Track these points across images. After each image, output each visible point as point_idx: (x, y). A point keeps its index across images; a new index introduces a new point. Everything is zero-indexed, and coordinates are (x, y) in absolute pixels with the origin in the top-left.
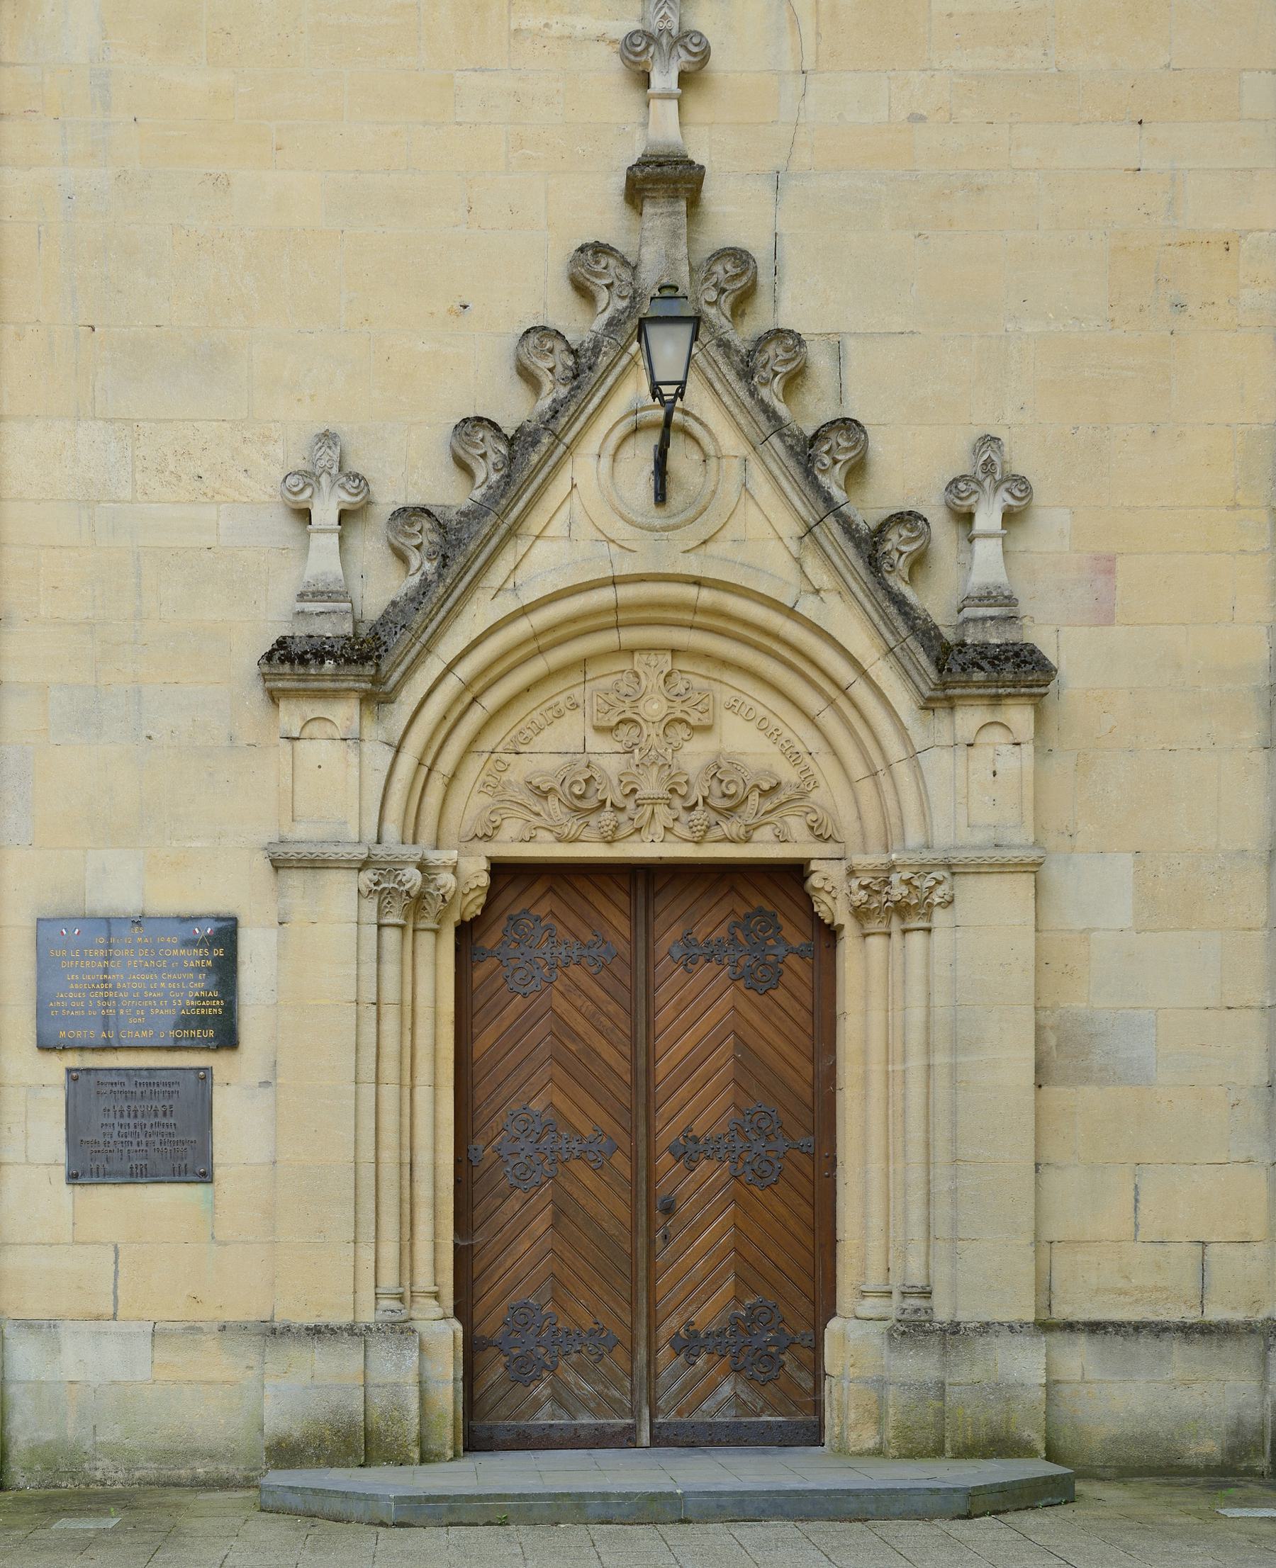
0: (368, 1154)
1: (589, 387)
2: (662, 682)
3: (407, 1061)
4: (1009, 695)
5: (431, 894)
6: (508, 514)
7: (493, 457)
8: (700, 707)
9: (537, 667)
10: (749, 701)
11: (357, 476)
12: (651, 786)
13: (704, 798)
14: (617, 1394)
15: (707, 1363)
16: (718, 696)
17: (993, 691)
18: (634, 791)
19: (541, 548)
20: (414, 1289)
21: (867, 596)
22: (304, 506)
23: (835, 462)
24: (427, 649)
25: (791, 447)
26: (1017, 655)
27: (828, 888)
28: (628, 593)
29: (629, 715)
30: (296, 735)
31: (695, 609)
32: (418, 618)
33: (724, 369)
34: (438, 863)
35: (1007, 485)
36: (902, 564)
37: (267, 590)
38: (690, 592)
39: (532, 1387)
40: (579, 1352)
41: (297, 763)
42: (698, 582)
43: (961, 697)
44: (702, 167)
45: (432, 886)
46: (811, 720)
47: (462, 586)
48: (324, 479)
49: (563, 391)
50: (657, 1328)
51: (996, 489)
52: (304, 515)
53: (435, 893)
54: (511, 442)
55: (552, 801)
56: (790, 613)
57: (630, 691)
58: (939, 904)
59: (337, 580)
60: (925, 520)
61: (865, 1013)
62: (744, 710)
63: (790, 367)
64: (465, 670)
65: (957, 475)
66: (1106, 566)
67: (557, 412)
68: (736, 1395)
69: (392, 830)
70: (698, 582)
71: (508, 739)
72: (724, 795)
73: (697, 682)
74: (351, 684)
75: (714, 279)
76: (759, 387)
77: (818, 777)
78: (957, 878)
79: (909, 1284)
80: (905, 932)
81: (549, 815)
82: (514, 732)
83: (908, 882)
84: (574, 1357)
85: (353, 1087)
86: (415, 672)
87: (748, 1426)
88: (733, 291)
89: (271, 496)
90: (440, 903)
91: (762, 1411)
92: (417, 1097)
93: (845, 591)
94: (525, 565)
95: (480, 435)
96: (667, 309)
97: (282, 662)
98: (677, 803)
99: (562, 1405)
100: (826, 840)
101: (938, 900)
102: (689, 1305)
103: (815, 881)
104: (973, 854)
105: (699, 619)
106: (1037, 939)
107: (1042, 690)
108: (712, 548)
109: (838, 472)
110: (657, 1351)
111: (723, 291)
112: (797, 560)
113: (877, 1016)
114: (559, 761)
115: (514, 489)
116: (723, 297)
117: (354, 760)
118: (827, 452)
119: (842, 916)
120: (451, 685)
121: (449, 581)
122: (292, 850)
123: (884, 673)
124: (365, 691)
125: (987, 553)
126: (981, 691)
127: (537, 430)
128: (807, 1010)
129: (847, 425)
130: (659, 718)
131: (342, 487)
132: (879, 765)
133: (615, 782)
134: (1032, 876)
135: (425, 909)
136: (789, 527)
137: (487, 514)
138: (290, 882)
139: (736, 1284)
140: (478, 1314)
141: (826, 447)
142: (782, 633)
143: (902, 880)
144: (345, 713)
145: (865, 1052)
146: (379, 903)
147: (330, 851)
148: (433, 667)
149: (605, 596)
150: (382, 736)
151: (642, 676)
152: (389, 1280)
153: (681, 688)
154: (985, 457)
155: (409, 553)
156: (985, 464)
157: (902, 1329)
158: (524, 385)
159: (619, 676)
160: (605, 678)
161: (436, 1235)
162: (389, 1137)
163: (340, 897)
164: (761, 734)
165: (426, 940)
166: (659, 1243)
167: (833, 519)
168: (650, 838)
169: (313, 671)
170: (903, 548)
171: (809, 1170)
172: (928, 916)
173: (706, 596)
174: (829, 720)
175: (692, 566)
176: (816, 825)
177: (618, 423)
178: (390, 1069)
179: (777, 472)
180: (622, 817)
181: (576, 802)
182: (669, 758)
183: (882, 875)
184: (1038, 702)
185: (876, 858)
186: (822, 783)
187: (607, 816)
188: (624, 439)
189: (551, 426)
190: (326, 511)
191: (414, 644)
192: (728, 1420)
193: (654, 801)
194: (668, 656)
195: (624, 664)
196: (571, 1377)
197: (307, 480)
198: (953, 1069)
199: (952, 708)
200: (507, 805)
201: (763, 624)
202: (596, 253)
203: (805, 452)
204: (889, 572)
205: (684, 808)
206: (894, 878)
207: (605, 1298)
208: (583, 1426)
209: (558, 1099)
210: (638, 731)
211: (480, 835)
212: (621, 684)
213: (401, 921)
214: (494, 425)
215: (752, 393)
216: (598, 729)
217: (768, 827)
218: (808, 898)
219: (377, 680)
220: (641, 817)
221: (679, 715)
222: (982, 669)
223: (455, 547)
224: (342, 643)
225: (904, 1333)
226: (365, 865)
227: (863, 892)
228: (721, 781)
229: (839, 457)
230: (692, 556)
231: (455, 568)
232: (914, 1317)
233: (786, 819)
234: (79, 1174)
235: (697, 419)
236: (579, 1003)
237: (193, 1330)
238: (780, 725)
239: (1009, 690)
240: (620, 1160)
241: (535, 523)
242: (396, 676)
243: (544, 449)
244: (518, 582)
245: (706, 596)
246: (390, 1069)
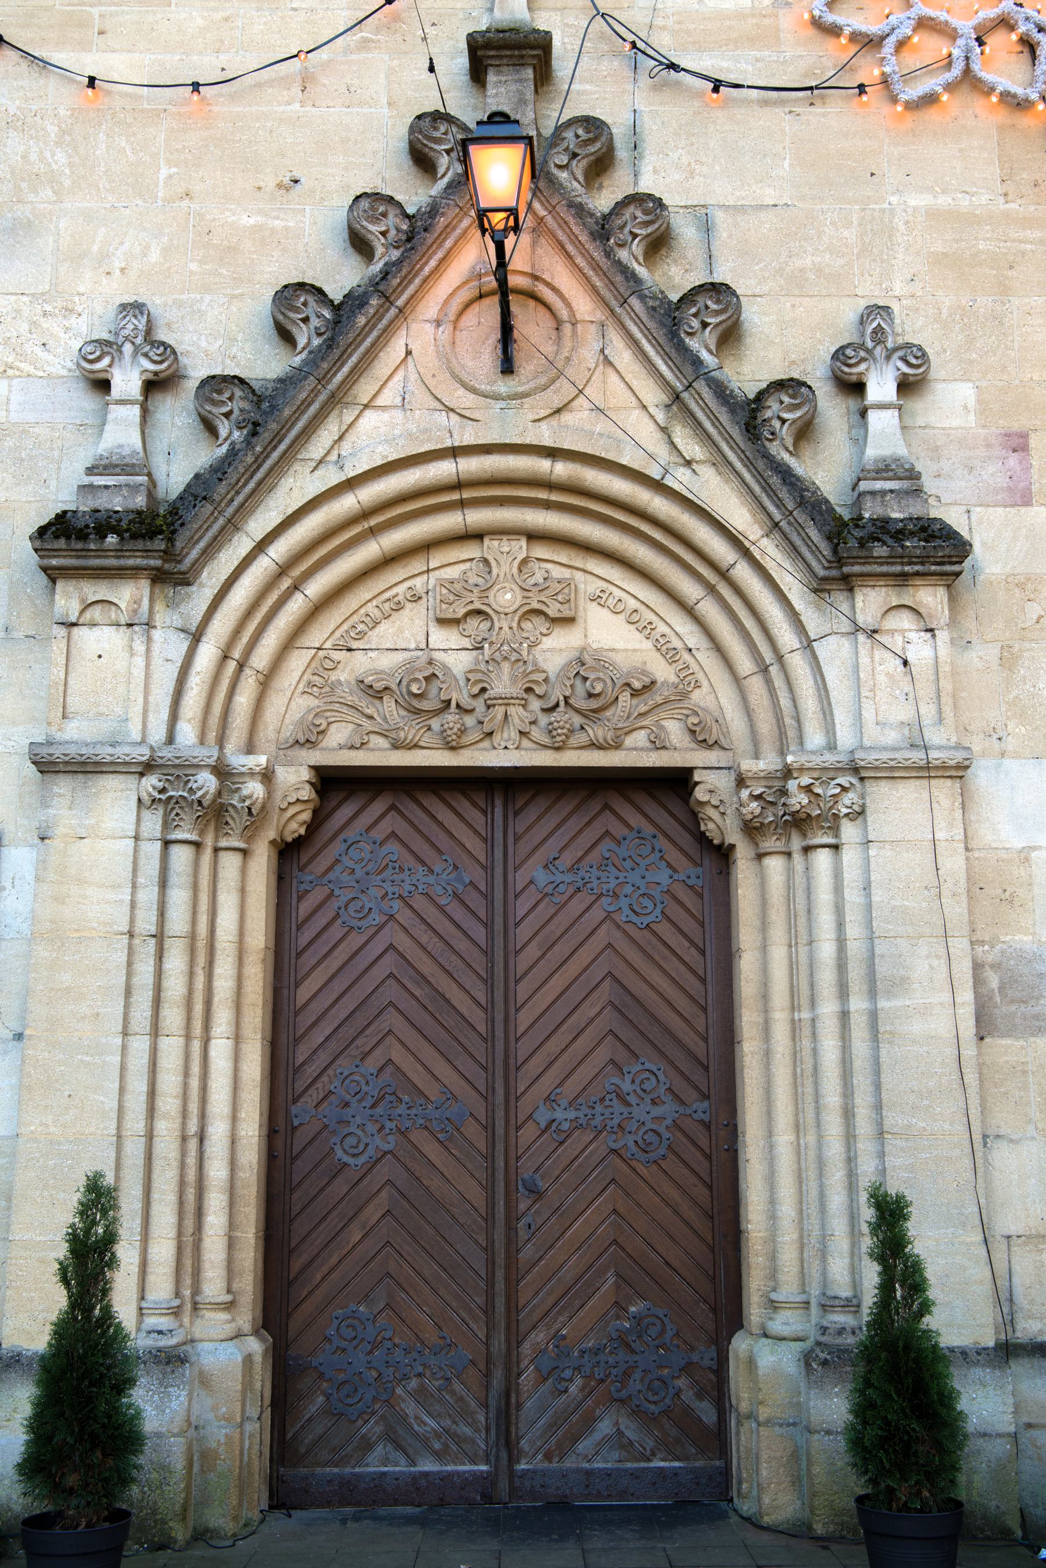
0: (136, 1124)
1: (425, 248)
2: (515, 570)
3: (198, 1007)
4: (917, 574)
5: (234, 806)
6: (331, 379)
7: (315, 322)
8: (560, 598)
9: (369, 551)
10: (617, 593)
11: (163, 343)
12: (502, 684)
13: (566, 698)
14: (467, 1430)
15: (582, 1390)
16: (582, 586)
17: (897, 569)
18: (483, 690)
19: (370, 418)
20: (198, 1298)
21: (745, 466)
22: (102, 376)
23: (705, 325)
24: (233, 525)
25: (654, 309)
26: (923, 529)
27: (714, 802)
28: (471, 466)
29: (477, 605)
30: (74, 620)
31: (550, 485)
32: (222, 488)
33: (576, 230)
34: (243, 770)
35: (900, 353)
36: (786, 433)
37: (59, 468)
38: (543, 466)
39: (360, 1422)
40: (419, 1375)
41: (74, 651)
42: (553, 453)
43: (862, 575)
44: (547, 33)
45: (236, 796)
46: (689, 611)
47: (275, 455)
48: (128, 348)
49: (395, 254)
50: (519, 1343)
51: (888, 358)
52: (103, 385)
53: (239, 806)
54: (336, 308)
55: (389, 704)
56: (658, 486)
57: (480, 581)
58: (847, 815)
59: (135, 453)
60: (810, 387)
61: (764, 948)
62: (611, 602)
63: (650, 230)
64: (279, 550)
65: (845, 343)
66: (1018, 444)
67: (387, 273)
68: (620, 1433)
69: (187, 733)
70: (553, 453)
71: (338, 634)
72: (590, 695)
73: (557, 572)
74: (139, 562)
75: (565, 144)
76: (616, 248)
77: (700, 676)
78: (867, 783)
79: (830, 1293)
80: (807, 850)
81: (385, 719)
82: (345, 627)
83: (808, 789)
84: (414, 1383)
85: (119, 1041)
86: (219, 551)
87: (634, 1475)
88: (587, 156)
89: (70, 370)
90: (246, 817)
91: (653, 1454)
92: (213, 1053)
93: (720, 462)
94: (350, 438)
95: (302, 299)
96: (515, 181)
97: (57, 537)
98: (535, 705)
99: (398, 1446)
100: (710, 747)
101: (845, 811)
102: (559, 1313)
103: (700, 794)
104: (885, 756)
105: (555, 497)
106: (967, 859)
107: (956, 568)
108: (566, 417)
109: (710, 336)
110: (519, 1375)
111: (575, 155)
112: (664, 430)
113: (778, 954)
114: (400, 657)
115: (337, 352)
116: (574, 162)
117: (140, 647)
118: (695, 315)
119: (734, 836)
120: (263, 566)
121: (258, 449)
122: (57, 752)
123: (770, 552)
124: (157, 569)
125: (882, 423)
126: (885, 569)
127: (365, 293)
128: (697, 948)
129: (718, 290)
130: (512, 609)
131: (146, 355)
132: (768, 656)
133: (462, 683)
134: (957, 784)
135: (227, 823)
136: (653, 395)
137: (305, 378)
138: (56, 789)
139: (617, 1287)
140: (295, 1324)
141: (693, 310)
142: (650, 510)
143: (800, 787)
144: (128, 595)
145: (765, 997)
146: (166, 815)
147: (105, 752)
148: (241, 546)
149: (444, 470)
150: (177, 621)
151: (493, 564)
153: (539, 578)
154: (875, 324)
155: (218, 422)
156: (875, 332)
157: (822, 1356)
158: (359, 258)
159: (468, 565)
160: (453, 566)
162: (168, 1103)
164: (632, 627)
165: (230, 863)
166: (523, 1235)
167: (703, 383)
168: (503, 744)
169: (92, 546)
170: (785, 416)
171: (704, 1142)
172: (835, 830)
173: (561, 470)
174: (709, 609)
175: (545, 435)
176: (698, 729)
177: (458, 288)
178: (172, 1017)
179: (638, 335)
180: (470, 721)
181: (415, 703)
182: (525, 653)
183: (777, 784)
184: (950, 579)
185: (768, 763)
186: (705, 684)
187: (451, 718)
188: (467, 305)
189: (381, 288)
190: (127, 381)
191: (216, 518)
192: (609, 1465)
193: (506, 701)
194: (523, 542)
195: (470, 550)
196: (410, 1408)
197: (106, 349)
198: (874, 1016)
199: (851, 590)
200: (336, 707)
201: (628, 500)
202: (435, 120)
203: (670, 319)
204: (770, 440)
205: (544, 710)
206: (792, 785)
207: (454, 1304)
208: (426, 1474)
209: (398, 1055)
210: (488, 624)
211: (302, 741)
212: (469, 574)
213: (194, 837)
214: (320, 291)
215: (608, 254)
216: (442, 622)
217: (643, 733)
218: (694, 815)
219: (168, 554)
220: (492, 720)
221: (535, 605)
222: (884, 543)
223: (262, 423)
224: (131, 517)
225: (825, 1363)
226: (147, 767)
227: (754, 805)
228: (585, 679)
229: (709, 320)
230: (544, 425)
231: (266, 436)
232: (839, 1341)
233: (663, 723)
235: (548, 284)
236: (424, 939)
238: (651, 617)
239: (917, 568)
240: (472, 1131)
241: (364, 390)
242: (194, 554)
243: (372, 311)
244: (343, 453)
245: (561, 470)
246: (172, 1017)
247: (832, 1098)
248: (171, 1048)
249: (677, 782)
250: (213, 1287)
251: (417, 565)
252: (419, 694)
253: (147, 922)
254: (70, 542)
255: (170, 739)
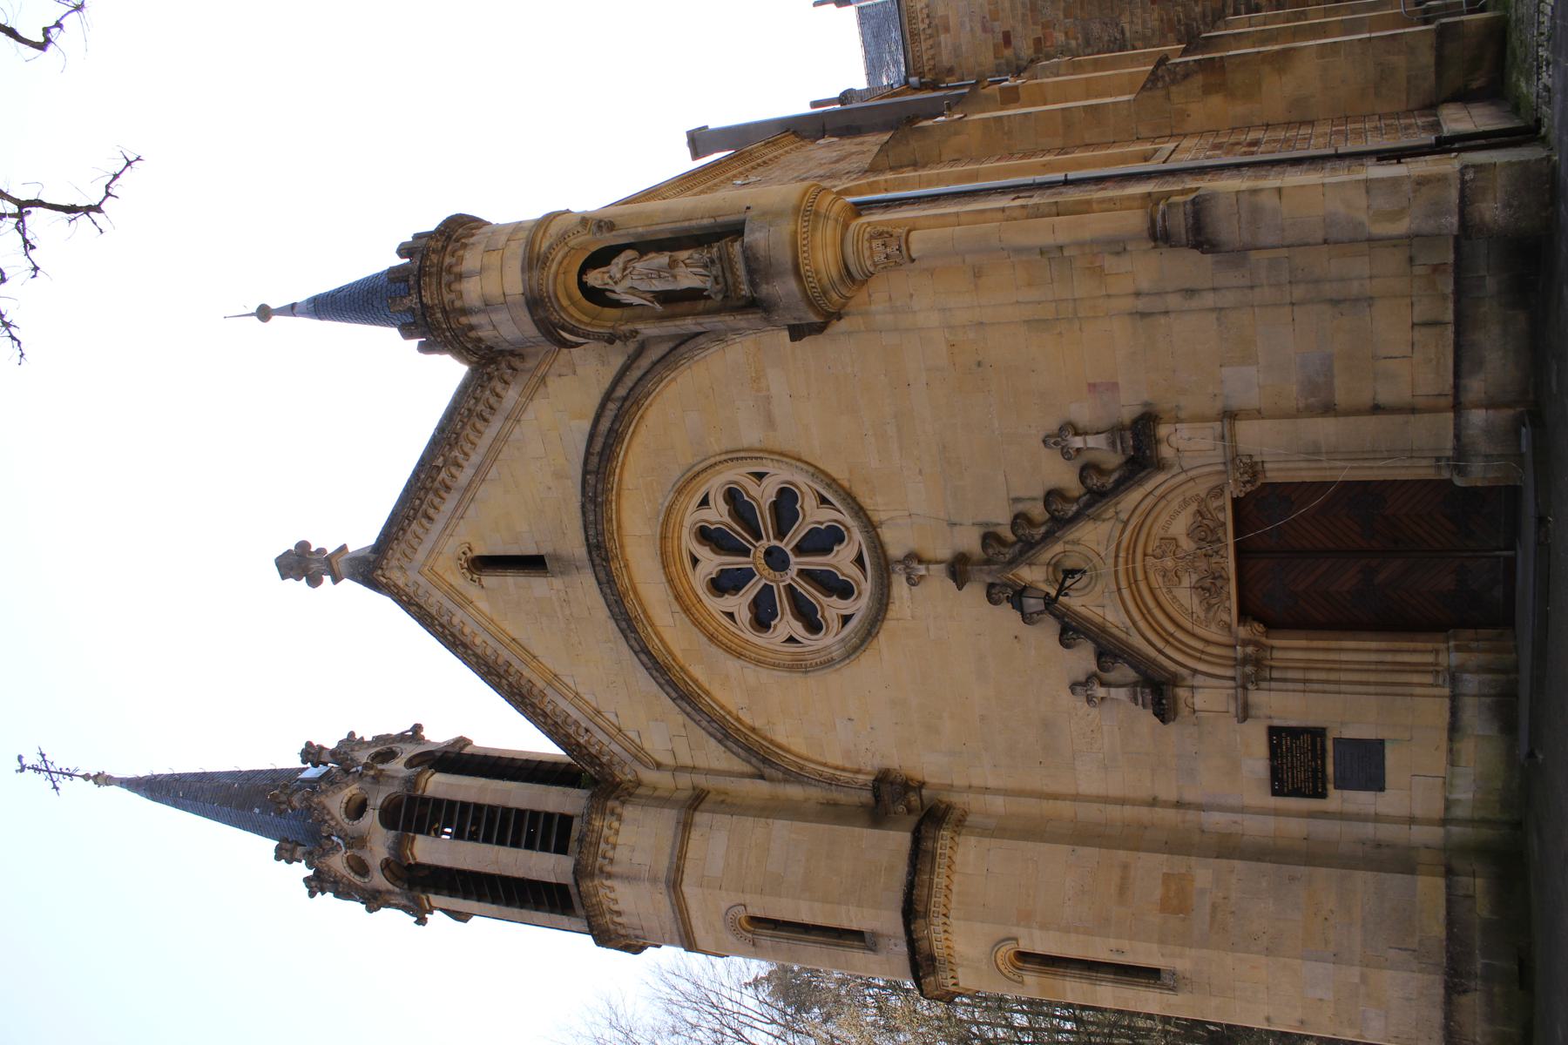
0: (1372, 689)
19: (1110, 618)
28: (1123, 584)
42: (1117, 556)
64: (1160, 645)
66: (1092, 387)
120: (1169, 651)
123: (1149, 486)
144: (1182, 693)
147: (1240, 702)
148: (1161, 658)
152: (1429, 679)
160: (1157, 580)
161: (1408, 651)
163: (1257, 697)
175: (1111, 561)
178: (1333, 676)
190: (1100, 692)
223: (1109, 651)
226: (1245, 688)
234: (1382, 789)
237: (1451, 751)
241: (1098, 620)
246: (1333, 676)
247: (1321, 656)
248: (1344, 677)
249: (1236, 502)
250: (1430, 658)
251: (1158, 592)
252: (1208, 588)
253: (1300, 686)
254: (1164, 710)
255: (1233, 679)
